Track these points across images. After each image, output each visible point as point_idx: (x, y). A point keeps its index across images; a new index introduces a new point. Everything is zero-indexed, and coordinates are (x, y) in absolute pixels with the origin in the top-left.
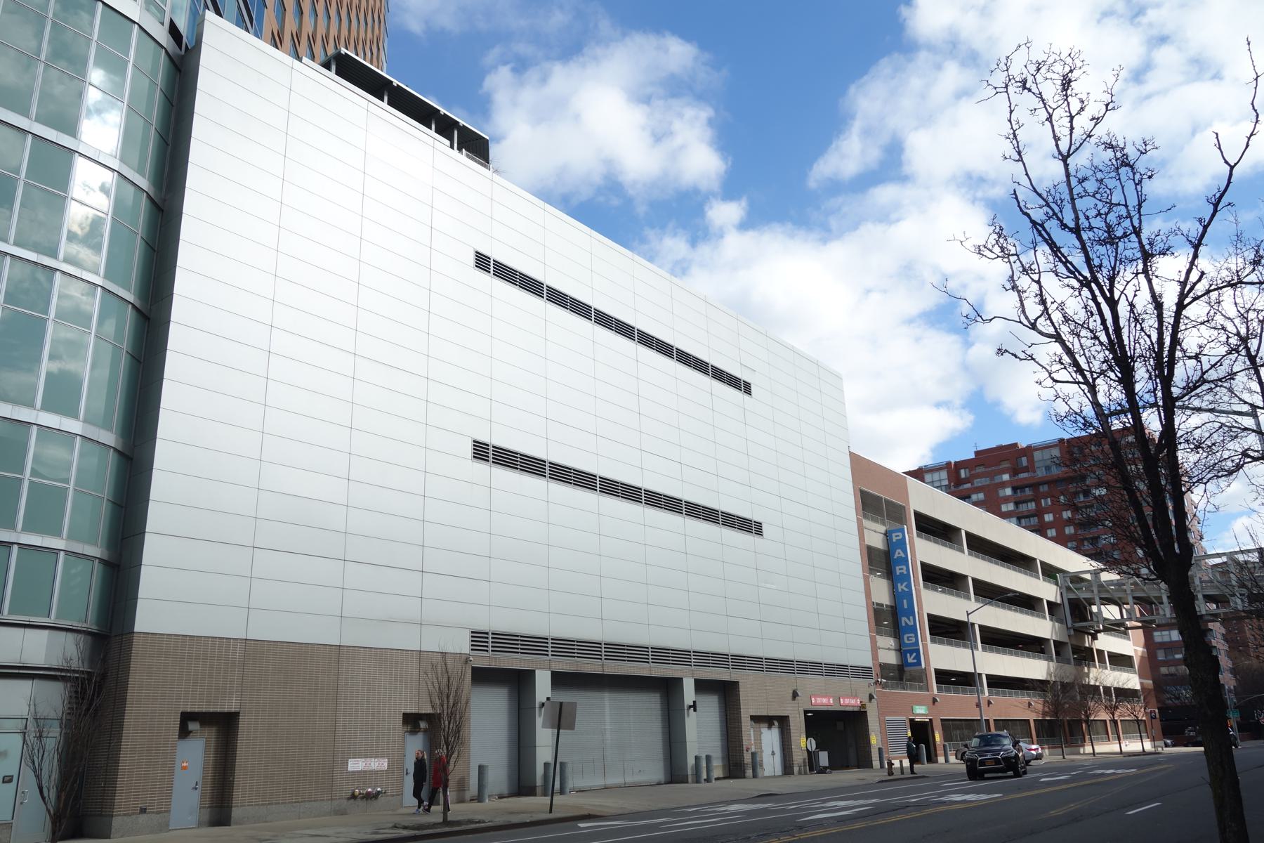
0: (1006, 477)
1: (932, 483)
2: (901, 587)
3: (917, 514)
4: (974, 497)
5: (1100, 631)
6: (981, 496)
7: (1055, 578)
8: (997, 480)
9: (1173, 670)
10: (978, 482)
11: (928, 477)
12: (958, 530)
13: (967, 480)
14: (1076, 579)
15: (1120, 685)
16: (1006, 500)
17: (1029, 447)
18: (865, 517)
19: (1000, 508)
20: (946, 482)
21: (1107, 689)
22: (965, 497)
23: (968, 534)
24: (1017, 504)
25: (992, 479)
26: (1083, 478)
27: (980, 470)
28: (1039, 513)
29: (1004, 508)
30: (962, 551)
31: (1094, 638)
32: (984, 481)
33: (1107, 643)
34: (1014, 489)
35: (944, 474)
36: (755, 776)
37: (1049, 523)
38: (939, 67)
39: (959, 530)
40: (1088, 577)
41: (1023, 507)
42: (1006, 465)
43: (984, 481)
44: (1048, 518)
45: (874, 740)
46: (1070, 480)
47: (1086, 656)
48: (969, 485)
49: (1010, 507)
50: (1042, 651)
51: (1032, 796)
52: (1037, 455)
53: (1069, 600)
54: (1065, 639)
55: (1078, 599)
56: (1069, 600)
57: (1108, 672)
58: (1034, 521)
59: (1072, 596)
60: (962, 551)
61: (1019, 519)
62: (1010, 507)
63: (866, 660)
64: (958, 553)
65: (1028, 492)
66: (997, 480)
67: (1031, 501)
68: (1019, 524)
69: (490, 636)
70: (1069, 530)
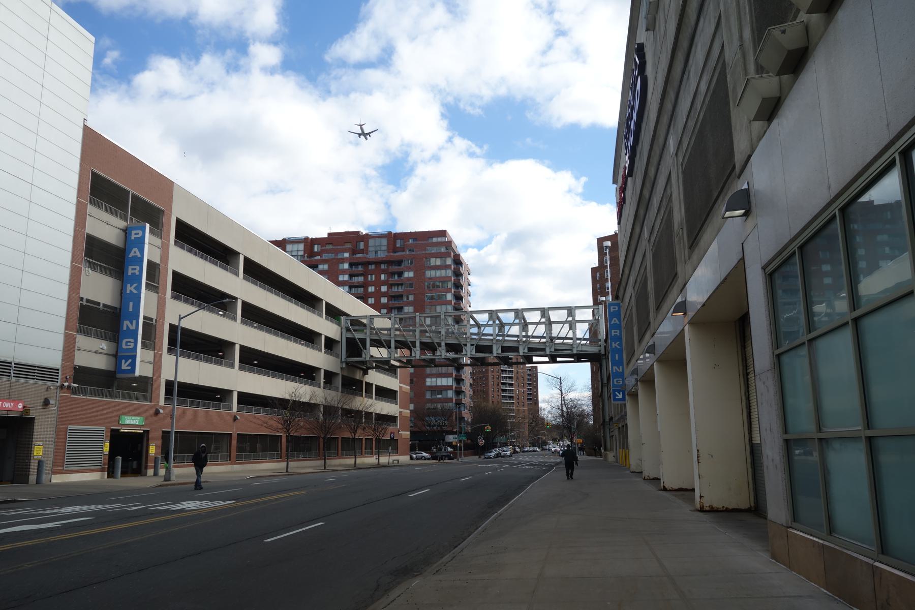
0: (346, 255)
1: (291, 252)
2: (130, 288)
3: (179, 223)
4: (321, 267)
5: (372, 368)
6: (326, 267)
7: (339, 320)
8: (340, 256)
9: (434, 406)
11: (289, 247)
13: (318, 254)
14: (356, 323)
15: (378, 412)
16: (344, 272)
17: (367, 235)
18: (92, 202)
19: (338, 278)
21: (369, 414)
22: (313, 266)
24: (351, 276)
26: (399, 263)
27: (329, 247)
28: (364, 286)
29: (341, 278)
30: (321, 316)
31: (365, 372)
33: (376, 378)
34: (351, 265)
35: (301, 247)
36: (38, 481)
37: (371, 293)
38: (571, 400)
39: (237, 254)
40: (364, 321)
41: (355, 279)
42: (348, 246)
44: (371, 289)
45: (38, 451)
46: (390, 263)
47: (353, 386)
48: (318, 258)
51: (25, 540)
52: (371, 242)
53: (347, 338)
54: (338, 371)
56: (347, 338)
57: (370, 401)
58: (361, 290)
59: (350, 336)
60: (321, 316)
61: (350, 288)
63: (53, 358)
64: (234, 277)
65: (360, 268)
66: (340, 256)
67: (361, 275)
68: (350, 292)
69: (13, 365)
70: (384, 300)
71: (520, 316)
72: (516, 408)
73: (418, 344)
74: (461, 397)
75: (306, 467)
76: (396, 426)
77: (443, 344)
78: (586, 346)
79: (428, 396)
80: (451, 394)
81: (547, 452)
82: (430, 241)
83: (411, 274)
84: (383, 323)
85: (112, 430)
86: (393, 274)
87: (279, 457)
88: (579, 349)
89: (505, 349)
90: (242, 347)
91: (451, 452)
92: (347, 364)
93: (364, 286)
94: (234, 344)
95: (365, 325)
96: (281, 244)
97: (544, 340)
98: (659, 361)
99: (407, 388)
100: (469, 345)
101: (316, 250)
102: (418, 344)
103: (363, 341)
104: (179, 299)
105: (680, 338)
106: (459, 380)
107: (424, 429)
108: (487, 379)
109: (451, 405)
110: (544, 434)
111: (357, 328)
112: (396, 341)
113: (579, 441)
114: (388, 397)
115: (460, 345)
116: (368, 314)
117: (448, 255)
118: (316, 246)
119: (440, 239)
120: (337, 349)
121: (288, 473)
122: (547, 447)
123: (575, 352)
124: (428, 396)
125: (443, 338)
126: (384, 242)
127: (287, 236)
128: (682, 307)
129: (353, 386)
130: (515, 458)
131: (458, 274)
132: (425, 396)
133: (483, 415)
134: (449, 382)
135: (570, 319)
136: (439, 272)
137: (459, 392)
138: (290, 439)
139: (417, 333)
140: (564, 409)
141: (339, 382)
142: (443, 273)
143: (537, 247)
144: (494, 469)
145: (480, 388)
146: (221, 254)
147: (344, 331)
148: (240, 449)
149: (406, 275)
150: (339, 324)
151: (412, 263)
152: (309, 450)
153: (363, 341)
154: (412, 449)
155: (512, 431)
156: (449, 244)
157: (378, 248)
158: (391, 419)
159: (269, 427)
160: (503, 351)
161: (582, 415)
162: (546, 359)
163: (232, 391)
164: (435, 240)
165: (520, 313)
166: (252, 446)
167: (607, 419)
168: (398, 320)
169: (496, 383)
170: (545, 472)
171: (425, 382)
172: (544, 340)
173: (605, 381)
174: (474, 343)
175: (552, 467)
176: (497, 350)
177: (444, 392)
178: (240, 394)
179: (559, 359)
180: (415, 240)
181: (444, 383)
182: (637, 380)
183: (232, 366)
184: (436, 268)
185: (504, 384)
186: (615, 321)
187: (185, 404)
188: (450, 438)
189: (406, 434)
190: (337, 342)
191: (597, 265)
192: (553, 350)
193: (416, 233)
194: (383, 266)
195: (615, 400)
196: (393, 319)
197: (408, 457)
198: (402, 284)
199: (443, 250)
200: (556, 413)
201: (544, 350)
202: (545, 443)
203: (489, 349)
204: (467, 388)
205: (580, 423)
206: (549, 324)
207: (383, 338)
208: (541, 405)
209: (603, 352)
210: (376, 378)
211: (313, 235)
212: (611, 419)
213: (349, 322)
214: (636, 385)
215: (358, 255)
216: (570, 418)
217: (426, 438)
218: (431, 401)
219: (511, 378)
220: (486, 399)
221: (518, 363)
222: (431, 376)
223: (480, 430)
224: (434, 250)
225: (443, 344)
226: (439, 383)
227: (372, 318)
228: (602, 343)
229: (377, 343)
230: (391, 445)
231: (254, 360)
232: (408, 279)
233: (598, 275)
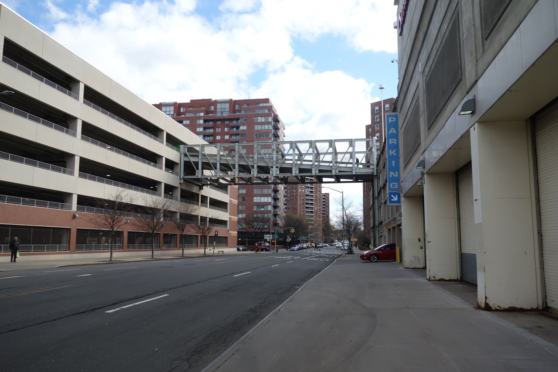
0: (202, 114)
1: (165, 112)
4: (185, 122)
5: (207, 185)
6: (188, 122)
7: (179, 148)
8: (198, 115)
10: (188, 115)
12: (77, 82)
13: (183, 113)
14: (191, 149)
16: (200, 126)
17: (216, 101)
19: (196, 130)
20: (172, 113)
22: (181, 122)
23: (167, 134)
24: (205, 128)
25: (195, 114)
26: (237, 119)
28: (213, 135)
31: (201, 188)
32: (192, 115)
33: (209, 192)
34: (205, 121)
35: (172, 108)
37: (218, 140)
40: (197, 148)
41: (208, 131)
42: (203, 108)
43: (192, 115)
44: (218, 138)
46: (231, 120)
47: (189, 197)
48: (183, 116)
49: (201, 129)
50: (155, 190)
52: (219, 106)
53: (185, 162)
55: (190, 162)
56: (185, 162)
57: (203, 209)
58: (211, 138)
62: (201, 129)
64: (161, 144)
65: (211, 123)
66: (198, 115)
67: (212, 128)
71: (313, 145)
72: (315, 220)
73: (237, 166)
74: (277, 210)
75: (138, 256)
76: (227, 227)
77: (255, 166)
78: (361, 170)
79: (255, 209)
80: (270, 208)
81: (333, 247)
82: (258, 106)
83: (245, 128)
84: (211, 150)
86: (233, 127)
87: (176, 247)
88: (358, 171)
89: (301, 170)
91: (267, 246)
92: (184, 180)
93: (213, 135)
95: (197, 152)
96: (159, 106)
97: (331, 165)
98: (485, 122)
99: (235, 201)
100: (274, 167)
101: (182, 111)
102: (237, 166)
103: (196, 164)
105: (464, 139)
106: (276, 199)
107: (249, 230)
108: (297, 200)
109: (271, 216)
110: (333, 236)
111: (192, 154)
112: (221, 164)
113: (354, 240)
114: (220, 207)
115: (268, 167)
116: (200, 144)
117: (269, 115)
118: (182, 109)
119: (264, 105)
120: (177, 169)
121: (183, 257)
122: (334, 244)
123: (354, 173)
124: (255, 209)
125: (255, 162)
126: (227, 106)
127: (163, 101)
128: (471, 106)
129: (189, 197)
130: (308, 253)
131: (276, 128)
132: (253, 208)
133: (290, 222)
134: (270, 200)
135: (351, 150)
136: (263, 126)
137: (275, 207)
138: (181, 236)
139: (236, 158)
140: (345, 217)
141: (178, 193)
142: (266, 127)
143: (330, 111)
144: (285, 261)
145: (291, 206)
146: (64, 82)
147: (183, 156)
148: (181, 242)
149: (241, 128)
150: (179, 151)
151: (245, 120)
152: (191, 243)
153: (196, 164)
154: (239, 243)
155: (311, 233)
156: (270, 108)
157: (223, 110)
158: (224, 223)
159: (96, 223)
160: (300, 172)
161: (358, 224)
162: (333, 180)
163: (71, 194)
164: (261, 105)
165: (313, 144)
166: (87, 239)
167: (377, 224)
168: (222, 148)
169: (302, 203)
170: (327, 264)
172: (331, 165)
173: (376, 195)
174: (279, 165)
175: (334, 258)
176: (295, 172)
177: (265, 207)
179: (342, 180)
180: (248, 104)
182: (423, 174)
183: (72, 173)
184: (262, 124)
185: (307, 204)
186: (393, 130)
187: (83, 210)
188: (268, 237)
189: (235, 233)
190: (177, 164)
191: (370, 123)
193: (248, 100)
194: (226, 122)
195: (391, 202)
196: (218, 147)
198: (238, 134)
199: (267, 111)
200: (340, 220)
201: (331, 171)
202: (333, 241)
203: (289, 170)
204: (281, 204)
205: (355, 228)
206: (336, 153)
207: (211, 161)
208: (331, 216)
209: (375, 174)
210: (209, 192)
211: (179, 101)
212: (381, 223)
213: (186, 149)
214: (422, 178)
215: (210, 115)
216: (349, 225)
217: (249, 238)
218: (256, 212)
219: (312, 200)
220: (295, 213)
221: (311, 183)
222: (257, 195)
223: (287, 232)
224: (261, 112)
225: (255, 166)
226: (262, 201)
227: (203, 146)
228: (375, 167)
229: (207, 166)
230: (222, 241)
231: (91, 169)
232: (243, 131)
233: (370, 130)
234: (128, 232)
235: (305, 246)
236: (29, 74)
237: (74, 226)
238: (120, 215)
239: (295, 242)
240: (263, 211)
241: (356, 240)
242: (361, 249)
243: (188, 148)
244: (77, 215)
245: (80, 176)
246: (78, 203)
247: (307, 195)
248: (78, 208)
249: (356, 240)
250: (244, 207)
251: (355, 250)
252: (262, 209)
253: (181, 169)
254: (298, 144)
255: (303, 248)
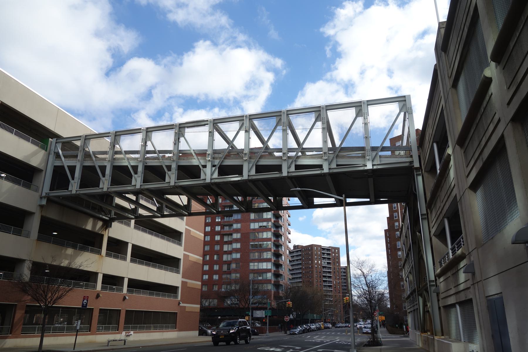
31: (107, 225)
40: (78, 143)
59: (58, 163)
76: (176, 297)
79: (251, 276)
80: (269, 275)
85: (100, 309)
90: (134, 246)
94: (127, 243)
95: (77, 148)
99: (196, 258)
100: (209, 165)
104: (138, 229)
108: (312, 273)
137: (277, 275)
141: (34, 225)
148: (127, 322)
160: (257, 171)
163: (123, 278)
165: (284, 118)
171: (249, 266)
178: (130, 280)
181: (265, 267)
185: (325, 277)
192: (334, 165)
197: (197, 333)
209: (416, 164)
216: (373, 300)
219: (330, 272)
222: (254, 261)
226: (261, 267)
234: (127, 311)
235: (313, 327)
236: (12, 132)
237: (123, 307)
238: (62, 283)
239: (295, 323)
240: (261, 280)
241: (383, 318)
242: (391, 332)
243: (64, 143)
244: (127, 298)
245: (132, 261)
246: (129, 286)
247: (324, 267)
248: (102, 288)
249: (383, 318)
250: (238, 275)
251: (382, 334)
252: (260, 278)
253: (45, 182)
254: (256, 122)
255: (309, 330)
